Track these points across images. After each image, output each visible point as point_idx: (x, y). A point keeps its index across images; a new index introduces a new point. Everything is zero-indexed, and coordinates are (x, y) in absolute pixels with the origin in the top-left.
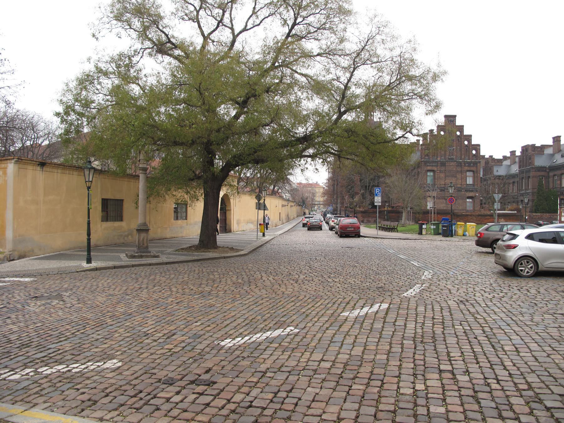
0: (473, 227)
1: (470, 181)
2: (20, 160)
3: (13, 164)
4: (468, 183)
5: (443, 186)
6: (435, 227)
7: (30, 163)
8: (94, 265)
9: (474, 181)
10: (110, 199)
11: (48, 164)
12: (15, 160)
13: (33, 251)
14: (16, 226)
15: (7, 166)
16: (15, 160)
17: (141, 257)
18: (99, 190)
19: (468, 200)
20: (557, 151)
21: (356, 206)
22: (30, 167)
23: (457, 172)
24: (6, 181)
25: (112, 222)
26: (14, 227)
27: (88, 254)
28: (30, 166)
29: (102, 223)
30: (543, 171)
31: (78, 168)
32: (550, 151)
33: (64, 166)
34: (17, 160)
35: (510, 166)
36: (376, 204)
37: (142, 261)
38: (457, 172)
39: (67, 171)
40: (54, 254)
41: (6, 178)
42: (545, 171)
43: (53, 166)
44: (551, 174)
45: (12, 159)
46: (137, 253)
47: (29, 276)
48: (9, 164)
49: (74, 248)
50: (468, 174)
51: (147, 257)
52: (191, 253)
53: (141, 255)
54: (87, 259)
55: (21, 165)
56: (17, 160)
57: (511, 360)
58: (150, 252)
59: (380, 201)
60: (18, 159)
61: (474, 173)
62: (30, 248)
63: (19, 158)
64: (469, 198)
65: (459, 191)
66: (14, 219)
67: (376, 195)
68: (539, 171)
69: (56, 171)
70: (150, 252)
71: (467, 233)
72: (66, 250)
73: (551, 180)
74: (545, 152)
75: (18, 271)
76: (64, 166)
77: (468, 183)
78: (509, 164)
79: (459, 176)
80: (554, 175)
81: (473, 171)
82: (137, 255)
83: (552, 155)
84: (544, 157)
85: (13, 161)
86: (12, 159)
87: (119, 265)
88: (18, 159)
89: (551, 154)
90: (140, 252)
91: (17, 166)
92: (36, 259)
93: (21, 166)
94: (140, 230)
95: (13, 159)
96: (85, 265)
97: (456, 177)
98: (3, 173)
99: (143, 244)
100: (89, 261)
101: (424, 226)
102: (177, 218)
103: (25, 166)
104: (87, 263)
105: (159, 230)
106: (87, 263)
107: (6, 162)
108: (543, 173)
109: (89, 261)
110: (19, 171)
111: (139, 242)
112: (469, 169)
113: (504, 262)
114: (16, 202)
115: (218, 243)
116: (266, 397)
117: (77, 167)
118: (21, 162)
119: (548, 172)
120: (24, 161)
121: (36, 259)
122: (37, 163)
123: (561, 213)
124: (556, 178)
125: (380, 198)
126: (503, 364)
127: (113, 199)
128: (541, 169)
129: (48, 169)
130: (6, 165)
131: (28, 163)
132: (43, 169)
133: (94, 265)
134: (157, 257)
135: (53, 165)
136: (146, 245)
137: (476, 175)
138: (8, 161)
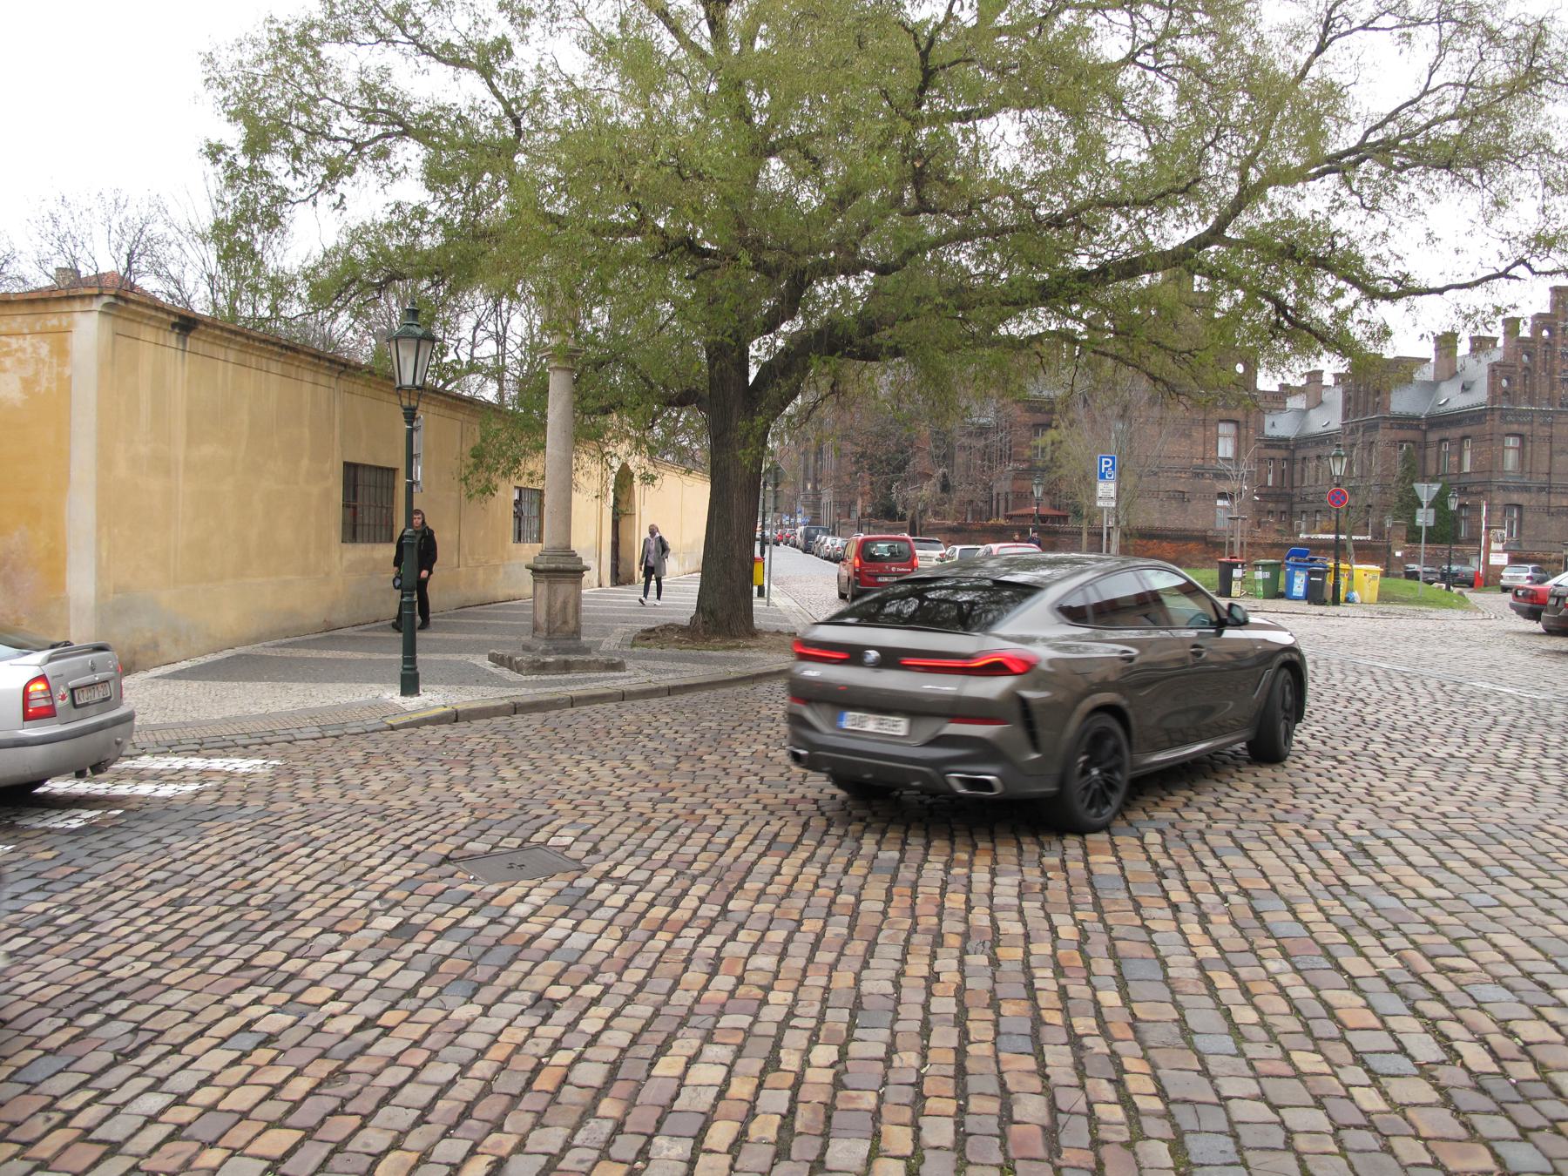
0: (1374, 578)
1: (1226, 448)
2: (121, 303)
3: (95, 316)
4: (1221, 454)
5: (1200, 462)
6: (1267, 575)
7: (151, 318)
8: (432, 699)
9: (1237, 450)
10: (364, 466)
11: (201, 327)
12: (106, 299)
13: (155, 645)
14: (104, 554)
15: (71, 324)
16: (106, 299)
17: (566, 667)
18: (337, 431)
19: (1220, 503)
20: (1447, 374)
21: (924, 511)
22: (148, 334)
23: (1193, 422)
24: (65, 384)
25: (369, 546)
26: (99, 558)
27: (405, 661)
28: (149, 329)
29: (345, 546)
30: (1411, 427)
31: (287, 348)
32: (1427, 373)
33: (248, 337)
34: (112, 300)
35: (1304, 412)
36: (1100, 504)
37: (569, 682)
38: (1193, 422)
39: (253, 359)
40: (219, 656)
41: (68, 371)
42: (1417, 428)
43: (216, 337)
44: (1433, 437)
45: (91, 296)
46: (546, 653)
47: (245, 751)
48: (78, 317)
49: (271, 636)
50: (1224, 429)
51: (586, 666)
52: (645, 650)
53: (566, 662)
54: (403, 678)
55: (120, 321)
56: (112, 300)
57: (1328, 921)
58: (587, 651)
59: (1113, 494)
60: (116, 296)
61: (1238, 428)
62: (149, 635)
63: (122, 293)
64: (1222, 496)
65: (1197, 475)
66: (99, 527)
67: (1103, 476)
68: (1401, 427)
69: (220, 352)
70: (587, 651)
71: (1355, 594)
72: (257, 640)
73: (1431, 452)
74: (1416, 376)
75: (173, 727)
76: (248, 337)
77: (1221, 454)
78: (1303, 406)
79: (1197, 434)
80: (1442, 440)
81: (1236, 422)
82: (550, 659)
83: (1433, 386)
84: (1413, 388)
85: (97, 305)
86: (91, 296)
87: (527, 700)
88: (116, 296)
89: (1429, 383)
90: (557, 651)
91: (108, 321)
92: (176, 676)
93: (122, 326)
94: (556, 570)
95: (99, 296)
96: (392, 695)
97: (1190, 436)
98: (51, 351)
99: (565, 622)
100: (410, 685)
101: (1237, 573)
102: (519, 537)
103: (133, 328)
104: (404, 693)
105: (481, 574)
106: (404, 693)
107: (65, 307)
108: (1409, 434)
109: (410, 685)
110: (114, 342)
111: (548, 614)
112: (1224, 414)
113: (621, 629)
114: (105, 462)
115: (756, 622)
116: (637, 1013)
117: (283, 346)
118: (121, 309)
119: (1425, 432)
120: (133, 307)
121: (176, 676)
122: (173, 319)
123: (1488, 542)
124: (1445, 447)
125: (1112, 487)
126: (1352, 943)
127: (371, 467)
128: (1405, 422)
129: (201, 347)
130: (65, 320)
131: (143, 315)
132: (185, 344)
133: (432, 699)
134: (616, 667)
135: (218, 332)
136: (572, 623)
137: (1244, 432)
138: (77, 306)
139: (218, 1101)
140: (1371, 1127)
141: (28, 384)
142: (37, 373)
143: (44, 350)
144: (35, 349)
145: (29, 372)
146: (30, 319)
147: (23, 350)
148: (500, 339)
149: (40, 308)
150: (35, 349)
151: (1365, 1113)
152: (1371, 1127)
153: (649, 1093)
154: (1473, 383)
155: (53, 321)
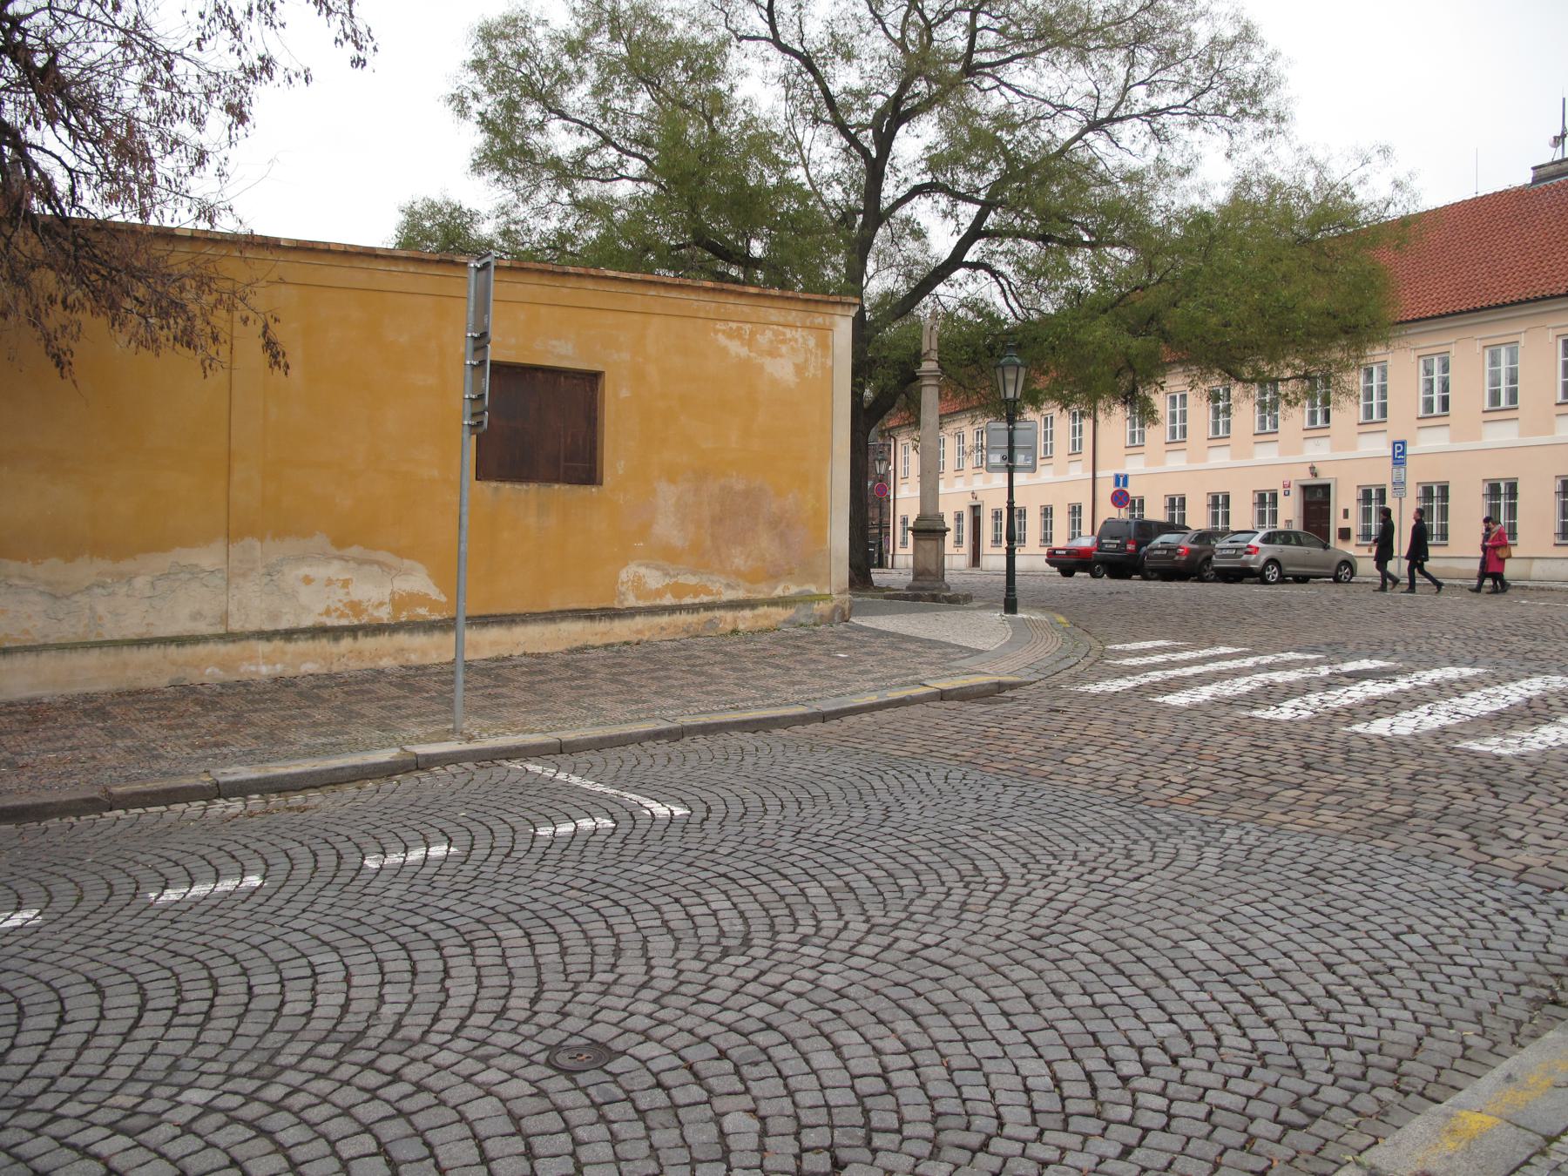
15: (832, 324)
107: (830, 309)
115: (391, 246)
138: (839, 310)
139: (761, 1030)
140: (770, 1027)
141: (800, 369)
142: (806, 360)
143: (812, 343)
144: (805, 341)
145: (800, 359)
146: (801, 314)
147: (796, 341)
148: (68, 66)
149: (812, 307)
150: (805, 341)
151: (761, 1020)
152: (770, 1027)
153: (500, 690)
154: (477, 167)
155: (819, 320)
